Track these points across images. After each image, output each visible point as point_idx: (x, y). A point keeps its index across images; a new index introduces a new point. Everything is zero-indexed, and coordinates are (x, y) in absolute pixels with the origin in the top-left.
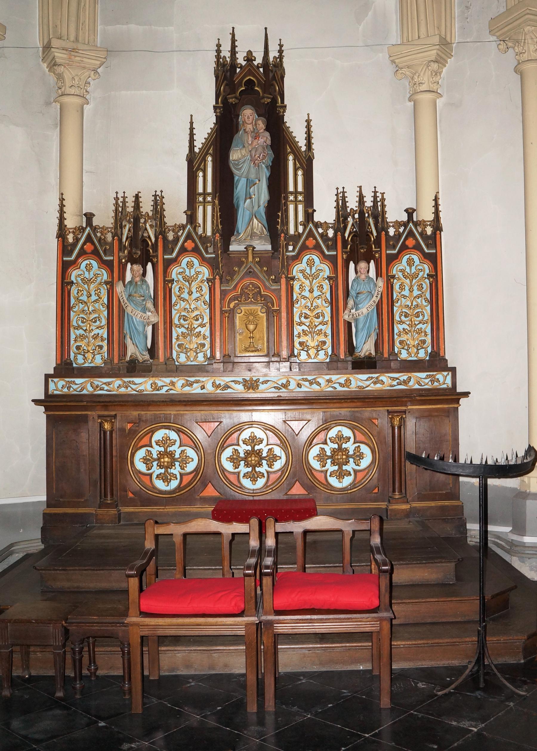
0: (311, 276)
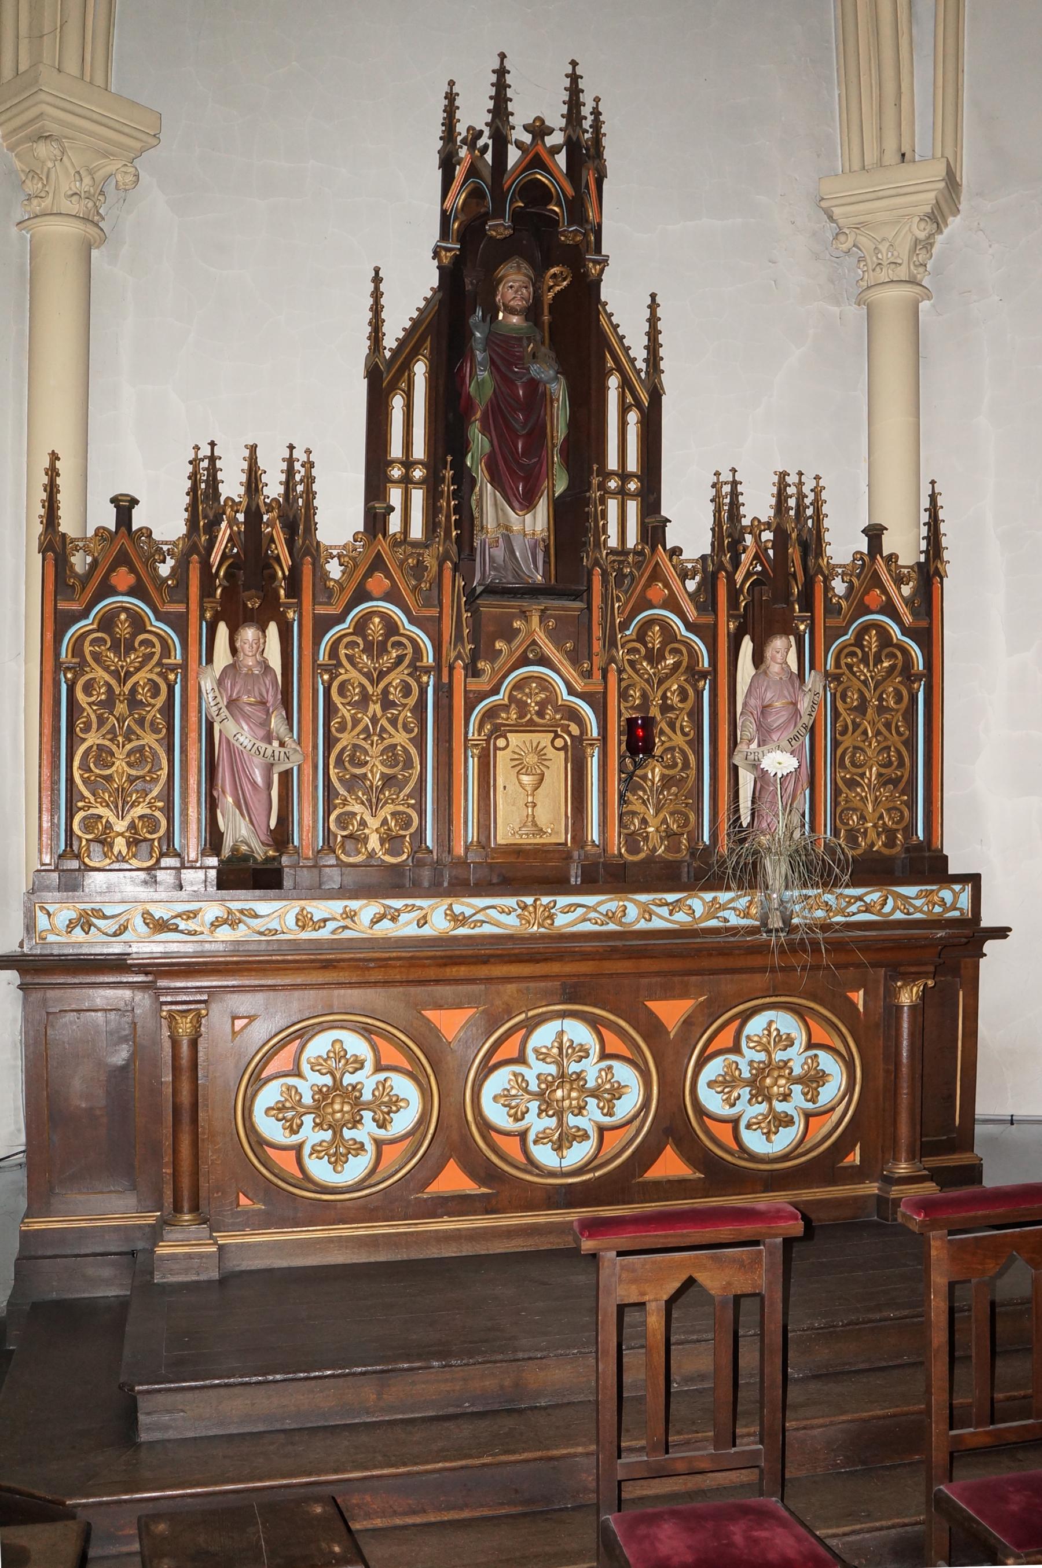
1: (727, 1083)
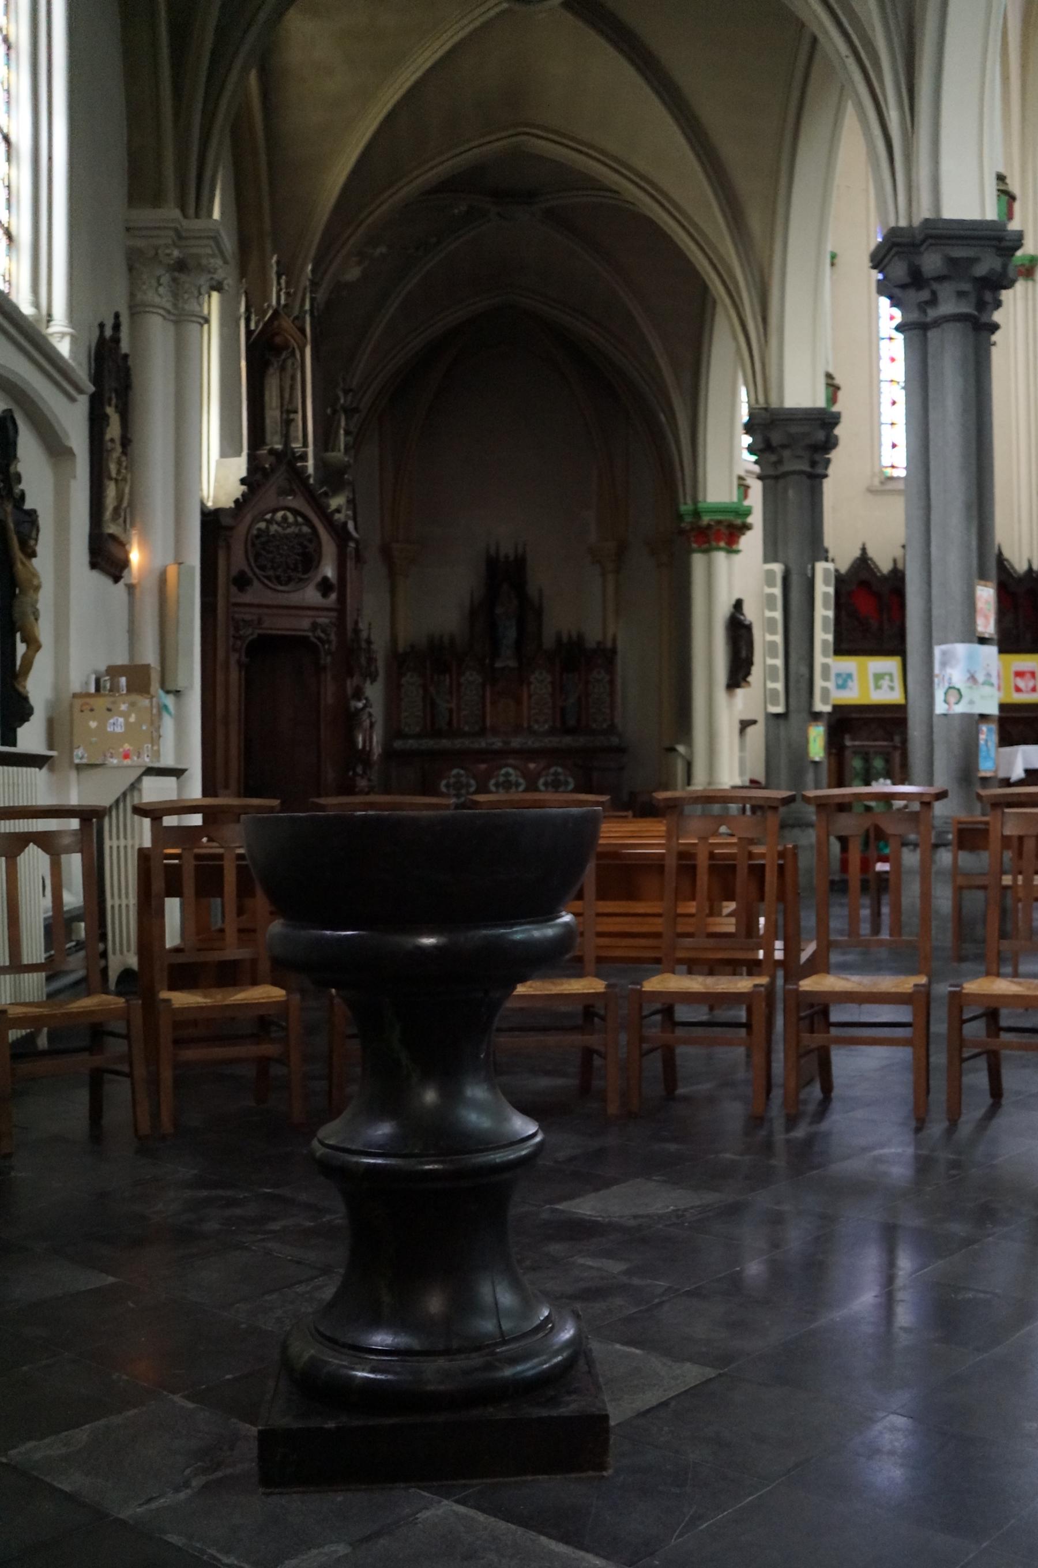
0: (540, 684)
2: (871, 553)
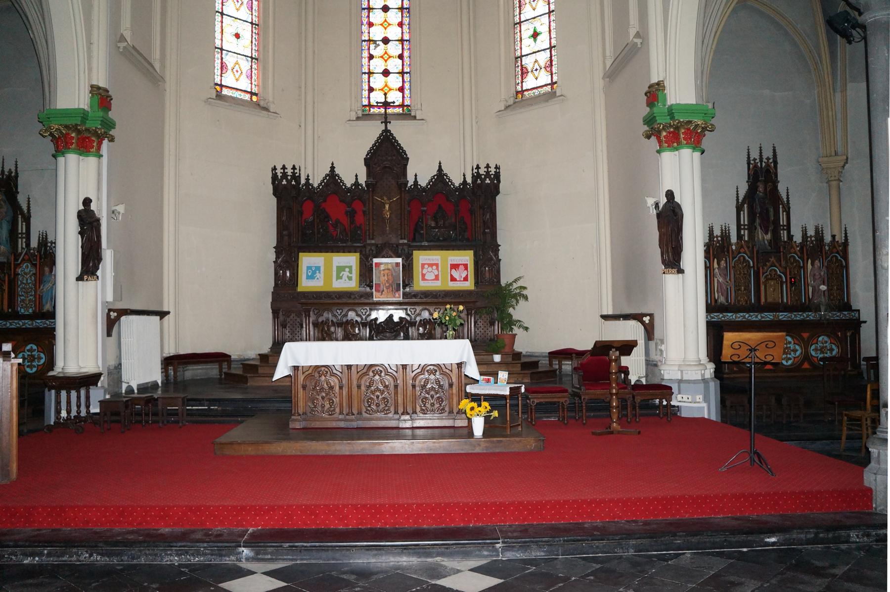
1: (816, 350)
2: (337, 171)
